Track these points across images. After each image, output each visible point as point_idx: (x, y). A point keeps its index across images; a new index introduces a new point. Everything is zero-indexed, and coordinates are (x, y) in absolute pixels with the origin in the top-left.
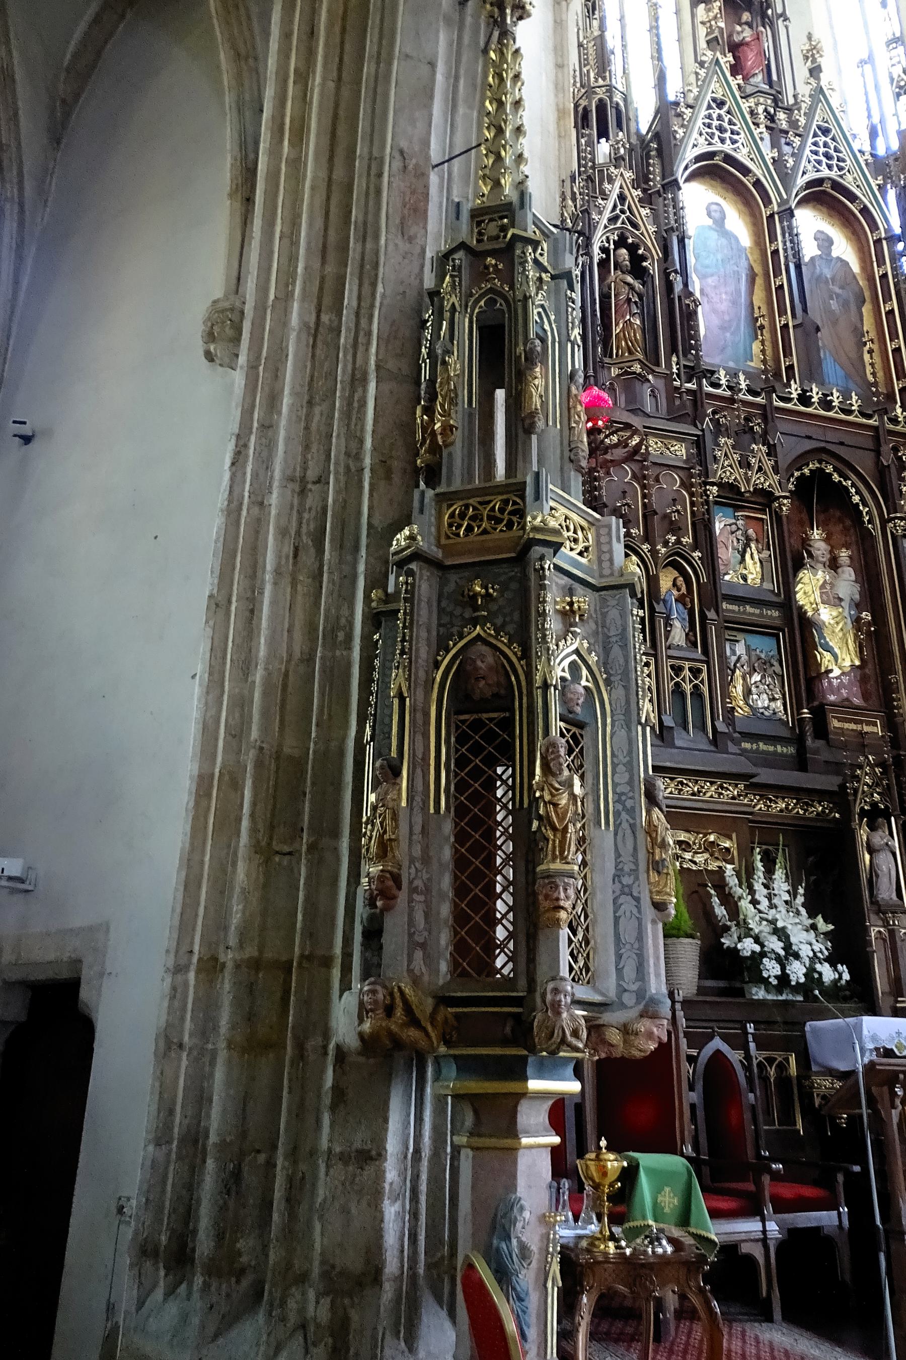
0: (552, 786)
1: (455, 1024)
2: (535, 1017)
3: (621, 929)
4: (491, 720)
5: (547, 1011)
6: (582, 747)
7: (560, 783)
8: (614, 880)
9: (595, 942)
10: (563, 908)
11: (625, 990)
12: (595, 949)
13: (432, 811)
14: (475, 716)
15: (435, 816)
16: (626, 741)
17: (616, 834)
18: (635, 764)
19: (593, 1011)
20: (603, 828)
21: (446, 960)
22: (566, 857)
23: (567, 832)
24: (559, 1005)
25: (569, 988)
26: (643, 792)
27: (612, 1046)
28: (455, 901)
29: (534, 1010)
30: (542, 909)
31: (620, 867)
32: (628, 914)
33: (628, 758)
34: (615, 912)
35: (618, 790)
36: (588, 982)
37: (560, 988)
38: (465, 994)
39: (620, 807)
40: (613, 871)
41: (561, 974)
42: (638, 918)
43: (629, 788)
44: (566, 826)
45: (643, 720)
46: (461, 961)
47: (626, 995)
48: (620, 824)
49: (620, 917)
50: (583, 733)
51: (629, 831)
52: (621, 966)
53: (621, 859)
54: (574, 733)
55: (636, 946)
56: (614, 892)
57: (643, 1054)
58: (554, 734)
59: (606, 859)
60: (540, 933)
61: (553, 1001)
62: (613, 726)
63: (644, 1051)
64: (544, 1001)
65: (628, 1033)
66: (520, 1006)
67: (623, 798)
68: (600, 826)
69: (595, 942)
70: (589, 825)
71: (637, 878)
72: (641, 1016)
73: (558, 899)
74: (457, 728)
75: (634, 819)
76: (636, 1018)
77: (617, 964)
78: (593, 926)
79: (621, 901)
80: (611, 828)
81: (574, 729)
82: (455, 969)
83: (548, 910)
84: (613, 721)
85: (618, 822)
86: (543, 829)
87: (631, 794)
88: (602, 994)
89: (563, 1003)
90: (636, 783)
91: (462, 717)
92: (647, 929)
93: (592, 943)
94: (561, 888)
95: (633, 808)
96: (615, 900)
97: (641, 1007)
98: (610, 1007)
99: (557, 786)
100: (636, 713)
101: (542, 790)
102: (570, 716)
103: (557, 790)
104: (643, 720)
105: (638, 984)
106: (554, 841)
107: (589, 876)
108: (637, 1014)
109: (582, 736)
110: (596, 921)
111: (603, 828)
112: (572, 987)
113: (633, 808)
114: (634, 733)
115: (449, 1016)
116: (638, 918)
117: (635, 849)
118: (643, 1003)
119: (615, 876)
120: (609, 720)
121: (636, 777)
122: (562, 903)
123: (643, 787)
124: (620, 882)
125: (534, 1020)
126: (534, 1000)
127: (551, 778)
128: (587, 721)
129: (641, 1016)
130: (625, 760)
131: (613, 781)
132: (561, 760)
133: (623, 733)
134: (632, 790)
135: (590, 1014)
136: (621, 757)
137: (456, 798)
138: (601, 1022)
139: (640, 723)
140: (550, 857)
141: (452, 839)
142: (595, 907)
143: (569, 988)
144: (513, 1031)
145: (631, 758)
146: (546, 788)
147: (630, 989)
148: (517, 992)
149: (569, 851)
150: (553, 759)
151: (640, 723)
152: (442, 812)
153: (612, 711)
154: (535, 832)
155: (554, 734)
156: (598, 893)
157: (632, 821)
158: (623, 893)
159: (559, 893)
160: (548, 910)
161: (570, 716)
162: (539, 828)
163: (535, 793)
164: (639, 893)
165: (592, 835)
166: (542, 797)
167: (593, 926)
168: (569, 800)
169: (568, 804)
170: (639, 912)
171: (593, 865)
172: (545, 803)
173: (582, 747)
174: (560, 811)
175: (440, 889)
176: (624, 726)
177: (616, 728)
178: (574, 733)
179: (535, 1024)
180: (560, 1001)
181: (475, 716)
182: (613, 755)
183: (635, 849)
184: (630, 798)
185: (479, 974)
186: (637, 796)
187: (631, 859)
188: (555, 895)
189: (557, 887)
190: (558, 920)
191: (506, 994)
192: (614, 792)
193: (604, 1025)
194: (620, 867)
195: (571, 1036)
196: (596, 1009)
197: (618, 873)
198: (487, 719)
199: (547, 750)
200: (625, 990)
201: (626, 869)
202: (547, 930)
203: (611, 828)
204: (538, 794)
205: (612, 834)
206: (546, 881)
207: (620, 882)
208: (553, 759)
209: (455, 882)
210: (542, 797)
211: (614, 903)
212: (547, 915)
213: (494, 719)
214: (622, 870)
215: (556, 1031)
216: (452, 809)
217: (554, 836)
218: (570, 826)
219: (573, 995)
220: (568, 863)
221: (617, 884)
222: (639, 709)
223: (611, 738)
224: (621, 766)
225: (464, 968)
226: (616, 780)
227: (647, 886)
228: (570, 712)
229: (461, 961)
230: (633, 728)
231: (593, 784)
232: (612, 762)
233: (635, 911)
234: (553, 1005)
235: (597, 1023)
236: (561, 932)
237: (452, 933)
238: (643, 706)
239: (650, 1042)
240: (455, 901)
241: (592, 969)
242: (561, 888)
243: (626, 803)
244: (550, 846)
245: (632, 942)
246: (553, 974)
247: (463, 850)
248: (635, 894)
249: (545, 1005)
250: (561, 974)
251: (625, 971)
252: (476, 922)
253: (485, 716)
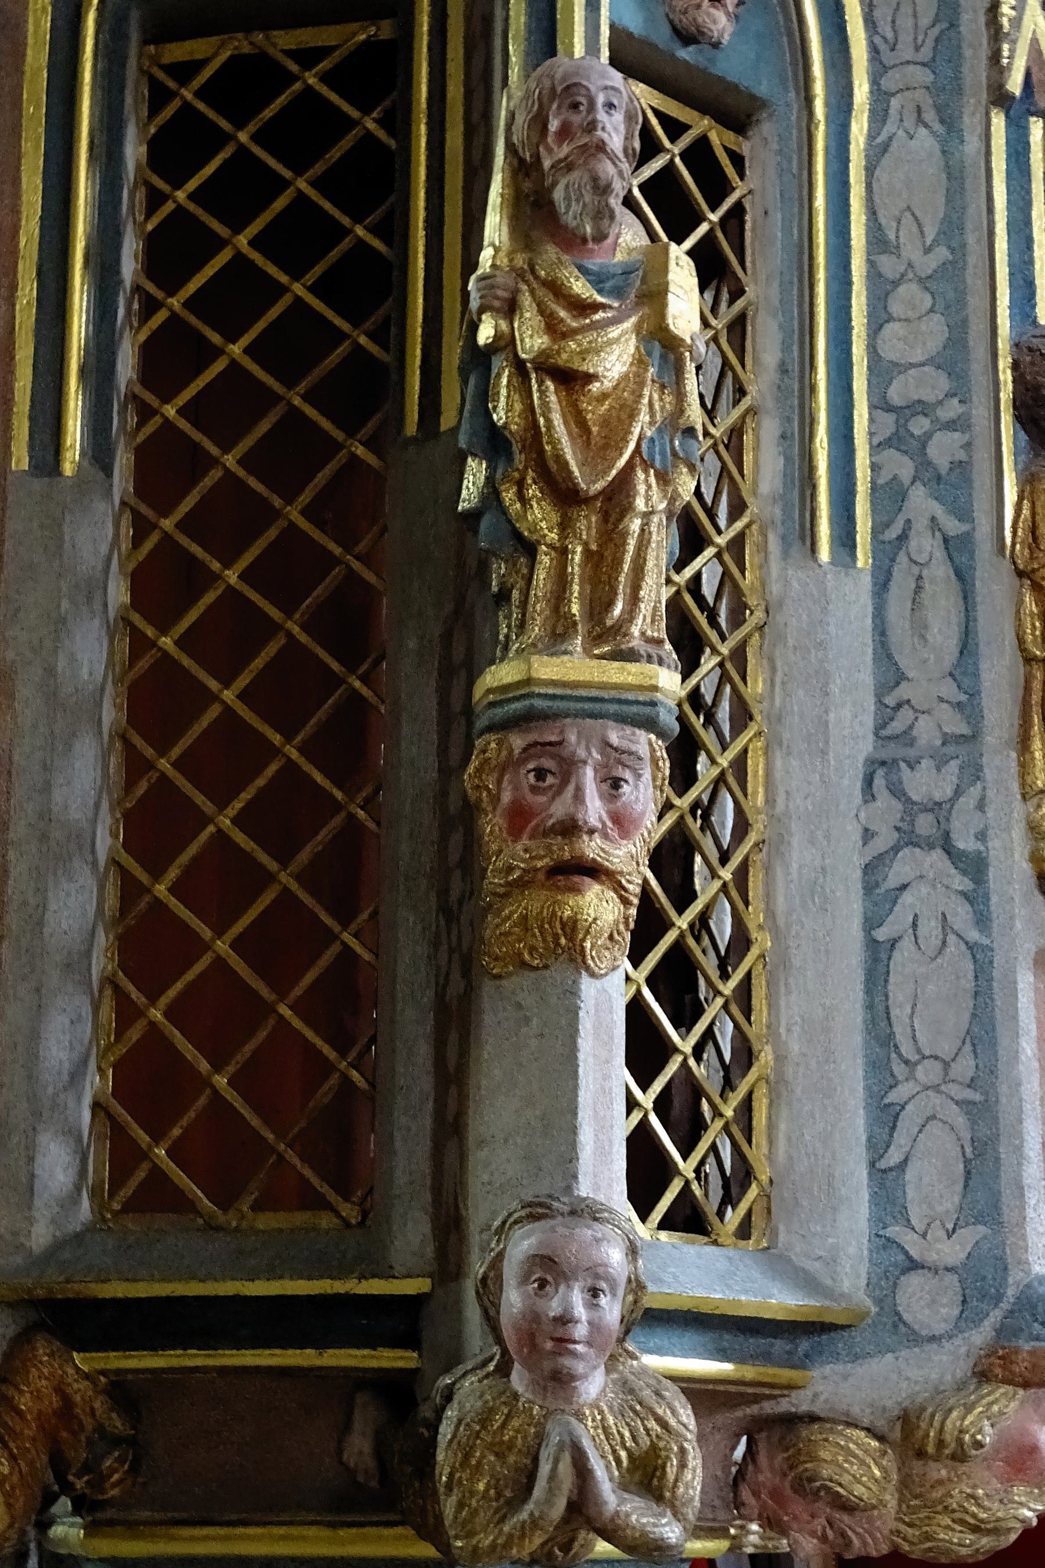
0: (557, 289)
1: (117, 1424)
2: (448, 1395)
3: (899, 994)
4: (307, 57)
5: (504, 1369)
6: (738, 210)
7: (597, 280)
8: (868, 781)
9: (780, 1058)
10: (595, 871)
11: (913, 1265)
12: (777, 1085)
13: (20, 458)
14: (239, 44)
15: (38, 485)
16: (933, 170)
17: (882, 583)
18: (974, 281)
19: (766, 1357)
20: (824, 554)
21: (72, 1133)
22: (620, 629)
23: (627, 509)
24: (563, 1342)
25: (615, 1256)
26: (1006, 394)
27: (847, 1506)
28: (124, 873)
29: (452, 1359)
30: (494, 880)
31: (897, 726)
32: (930, 928)
33: (942, 253)
34: (870, 924)
35: (895, 394)
36: (744, 1231)
37: (570, 1255)
38: (142, 1290)
39: (903, 467)
40: (866, 746)
41: (584, 1189)
42: (971, 947)
43: (943, 383)
44: (624, 482)
45: (1015, 84)
46: (143, 1137)
47: (914, 1284)
48: (903, 537)
49: (893, 943)
50: (745, 148)
51: (940, 571)
52: (893, 1157)
53: (904, 691)
54: (703, 141)
55: (965, 1067)
56: (868, 835)
57: (986, 1542)
58: (579, 51)
59: (835, 689)
60: (488, 987)
61: (533, 1317)
62: (879, 115)
63: (995, 1532)
64: (492, 1322)
65: (921, 1454)
66: (410, 1340)
67: (919, 426)
68: (814, 549)
69: (780, 1058)
70: (763, 548)
71: (973, 772)
72: (983, 1375)
73: (571, 828)
74: (159, 96)
75: (964, 515)
76: (960, 1387)
77: (877, 1148)
78: (771, 984)
79: (900, 870)
80: (863, 558)
81: (701, 124)
82: (119, 1175)
83: (522, 884)
84: (880, 97)
85: (893, 533)
86: (508, 495)
87: (952, 409)
88: (808, 1282)
89: (581, 1331)
90: (979, 353)
91: (178, 52)
92: (1013, 994)
93: (766, 1057)
94: (589, 774)
95: (962, 468)
96: (873, 870)
97: (981, 1336)
98: (840, 1342)
99: (580, 287)
100: (984, 52)
101: (510, 309)
102: (685, 54)
103: (583, 308)
104: (1015, 84)
105: (971, 1234)
106: (562, 553)
107: (756, 765)
108: (963, 1369)
109: (738, 161)
110: (784, 963)
111: (824, 554)
112: (633, 1251)
113: (962, 468)
114: (972, 145)
115: (80, 1390)
116: (971, 947)
117: (967, 645)
118: (996, 1316)
119: (874, 766)
120: (861, 91)
121: (977, 327)
122: (592, 848)
123: (1006, 376)
124: (897, 791)
125: (439, 1413)
126: (456, 1310)
127: (551, 252)
128: (763, 89)
129: (983, 1375)
130: (929, 264)
131: (872, 349)
132: (606, 169)
133: (925, 142)
134: (960, 391)
135: (749, 1372)
136: (911, 251)
137: (145, 412)
138: (800, 1402)
139: (1000, 98)
140: (536, 630)
141: (119, 593)
142: (781, 904)
143: (615, 1256)
144: (380, 1451)
145: (959, 251)
146: (526, 300)
147: (932, 1258)
148: (389, 1274)
149: (634, 600)
150: (567, 166)
151: (1000, 98)
152: (68, 469)
153: (874, 50)
154: (473, 516)
155: (579, 51)
156: (796, 841)
157: (953, 526)
158: (907, 838)
159: (579, 796)
160: (522, 884)
161: (685, 54)
162: (491, 491)
163: (474, 328)
164: (982, 836)
165: (775, 589)
166: (505, 343)
167: (771, 984)
168: (640, 362)
169: (633, 381)
170: (982, 921)
171: (776, 719)
172: (520, 367)
173: (738, 210)
174: (594, 413)
175: (45, 815)
176: (930, 116)
177: (889, 128)
178: (703, 141)
179: (446, 1430)
180: (565, 1320)
181: (239, 44)
182: (877, 241)
183: (967, 645)
184: (951, 425)
185: (225, 1203)
186: (980, 413)
187: (949, 689)
188: (559, 810)
189: (568, 768)
190: (572, 928)
191: (339, 1287)
192: (879, 404)
193: (813, 1418)
194: (897, 726)
195: (623, 1486)
196: (780, 1346)
197: (892, 751)
198: (289, 53)
199: (540, 122)
200: (913, 1265)
201: (926, 732)
202: (519, 984)
203: (863, 558)
204: (485, 333)
205: (866, 581)
206: (517, 742)
207: (897, 791)
208: (567, 166)
209: (129, 785)
210: (505, 343)
211: (869, 888)
212: (514, 910)
213: (323, 52)
214: (906, 738)
215: (545, 1469)
216: (123, 460)
217: (565, 526)
218: (646, 486)
219: (636, 1286)
220: (630, 656)
221: (884, 799)
222: (996, 34)
223: (870, 170)
224: (909, 290)
225: (157, 1174)
226: (891, 350)
227: (1019, 810)
228: (687, 37)
229: (143, 1137)
230: (970, 122)
231: (783, 369)
232: (874, 274)
233: (961, 915)
234: (530, 1337)
235: (784, 1406)
236: (588, 987)
237: (108, 1012)
238: (1017, 23)
239: (1019, 1493)
240: (124, 873)
241: (763, 1173)
242: (589, 774)
243: (932, 451)
244: (541, 575)
245: (946, 1049)
246: (540, 1189)
247: (166, 642)
248: (964, 843)
249: (499, 1340)
250: (584, 1189)
251: (910, 1174)
252: (220, 961)
253: (285, 40)
